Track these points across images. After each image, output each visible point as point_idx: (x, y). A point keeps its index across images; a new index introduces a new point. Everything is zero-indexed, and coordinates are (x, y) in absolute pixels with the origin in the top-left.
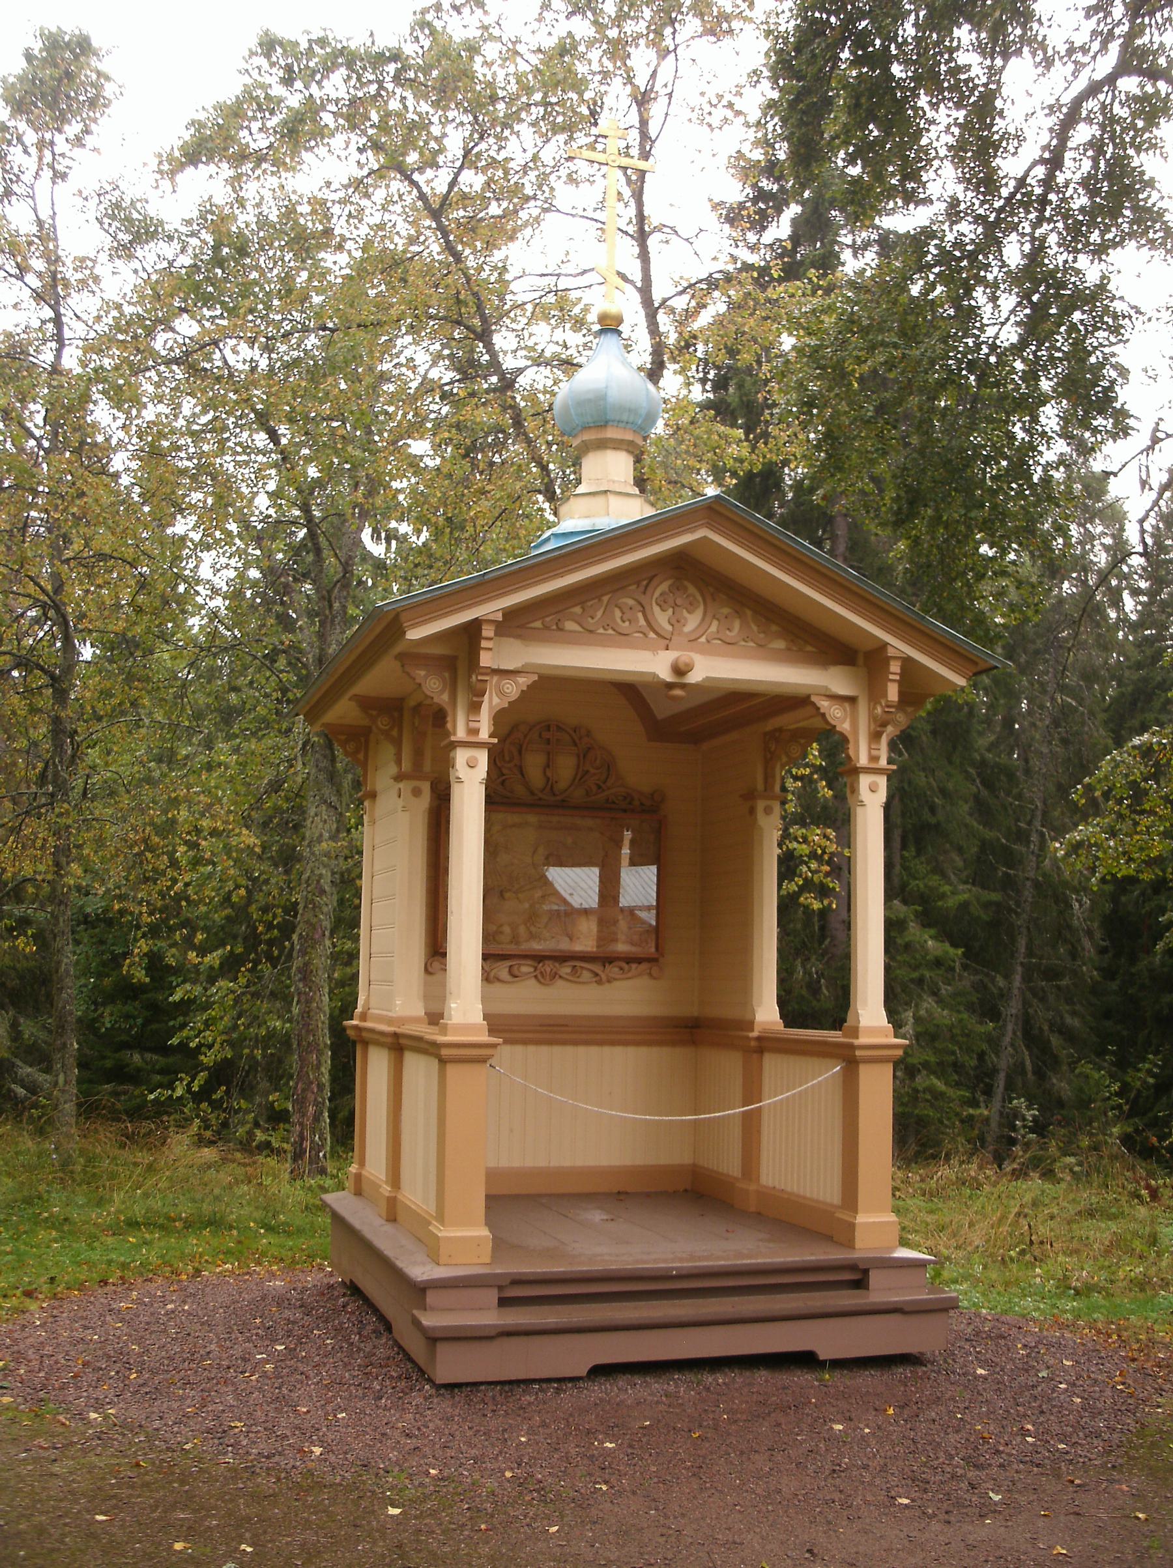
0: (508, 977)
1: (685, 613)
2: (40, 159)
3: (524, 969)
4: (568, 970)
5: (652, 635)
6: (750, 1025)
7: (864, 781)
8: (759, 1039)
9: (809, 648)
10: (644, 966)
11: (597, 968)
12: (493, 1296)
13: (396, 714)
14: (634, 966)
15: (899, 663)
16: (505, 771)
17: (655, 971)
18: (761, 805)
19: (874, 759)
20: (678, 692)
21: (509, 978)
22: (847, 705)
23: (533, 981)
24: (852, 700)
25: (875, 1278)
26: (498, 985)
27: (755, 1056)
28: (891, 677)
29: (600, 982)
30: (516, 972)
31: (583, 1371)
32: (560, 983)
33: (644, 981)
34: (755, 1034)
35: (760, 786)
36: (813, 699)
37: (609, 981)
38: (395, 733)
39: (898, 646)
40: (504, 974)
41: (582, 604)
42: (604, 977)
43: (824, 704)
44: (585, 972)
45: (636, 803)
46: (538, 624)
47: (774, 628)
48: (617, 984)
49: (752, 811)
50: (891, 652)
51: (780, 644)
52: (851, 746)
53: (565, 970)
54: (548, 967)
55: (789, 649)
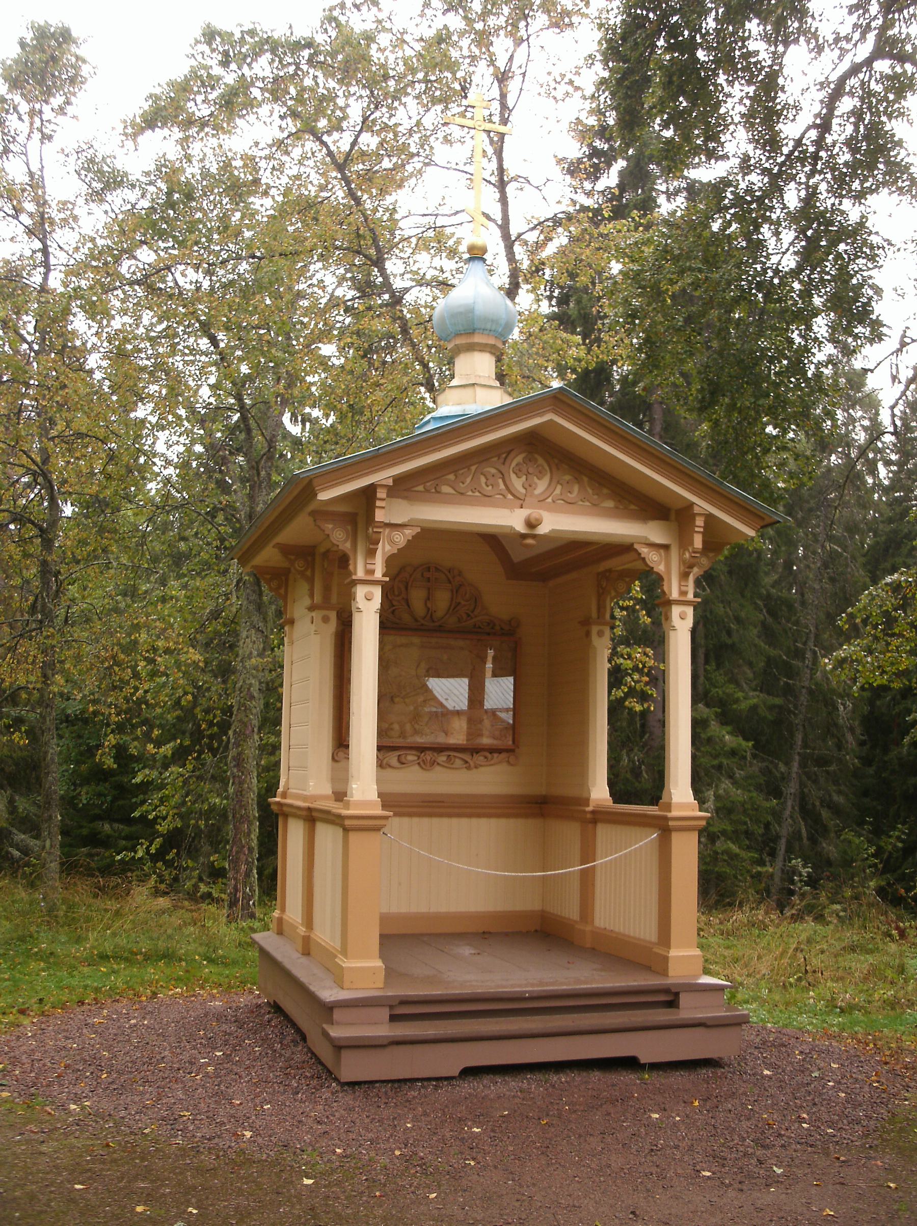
0: (397, 764)
1: (536, 479)
2: (32, 124)
3: (410, 758)
4: (444, 758)
5: (510, 496)
6: (587, 801)
7: (676, 611)
8: (593, 812)
9: (633, 507)
10: (503, 755)
11: (466, 757)
12: (385, 1013)
13: (309, 558)
14: (496, 755)
15: (703, 519)
16: (395, 603)
17: (512, 759)
18: (595, 629)
19: (683, 593)
20: (530, 541)
21: (398, 765)
22: (662, 551)
23: (417, 767)
24: (666, 547)
25: (684, 999)
26: (389, 770)
27: (590, 825)
28: (697, 529)
29: (469, 768)
30: (403, 760)
31: (456, 1072)
32: (438, 768)
33: (504, 767)
34: (590, 808)
35: (594, 614)
36: (636, 546)
37: (476, 767)
38: (309, 573)
39: (702, 505)
40: (394, 762)
41: (455, 472)
42: (472, 764)
43: (644, 551)
44: (457, 760)
45: (497, 628)
46: (421, 488)
47: (605, 491)
48: (482, 769)
49: (588, 634)
50: (696, 510)
51: (610, 504)
52: (665, 583)
53: (442, 758)
54: (428, 756)
55: (616, 508)
